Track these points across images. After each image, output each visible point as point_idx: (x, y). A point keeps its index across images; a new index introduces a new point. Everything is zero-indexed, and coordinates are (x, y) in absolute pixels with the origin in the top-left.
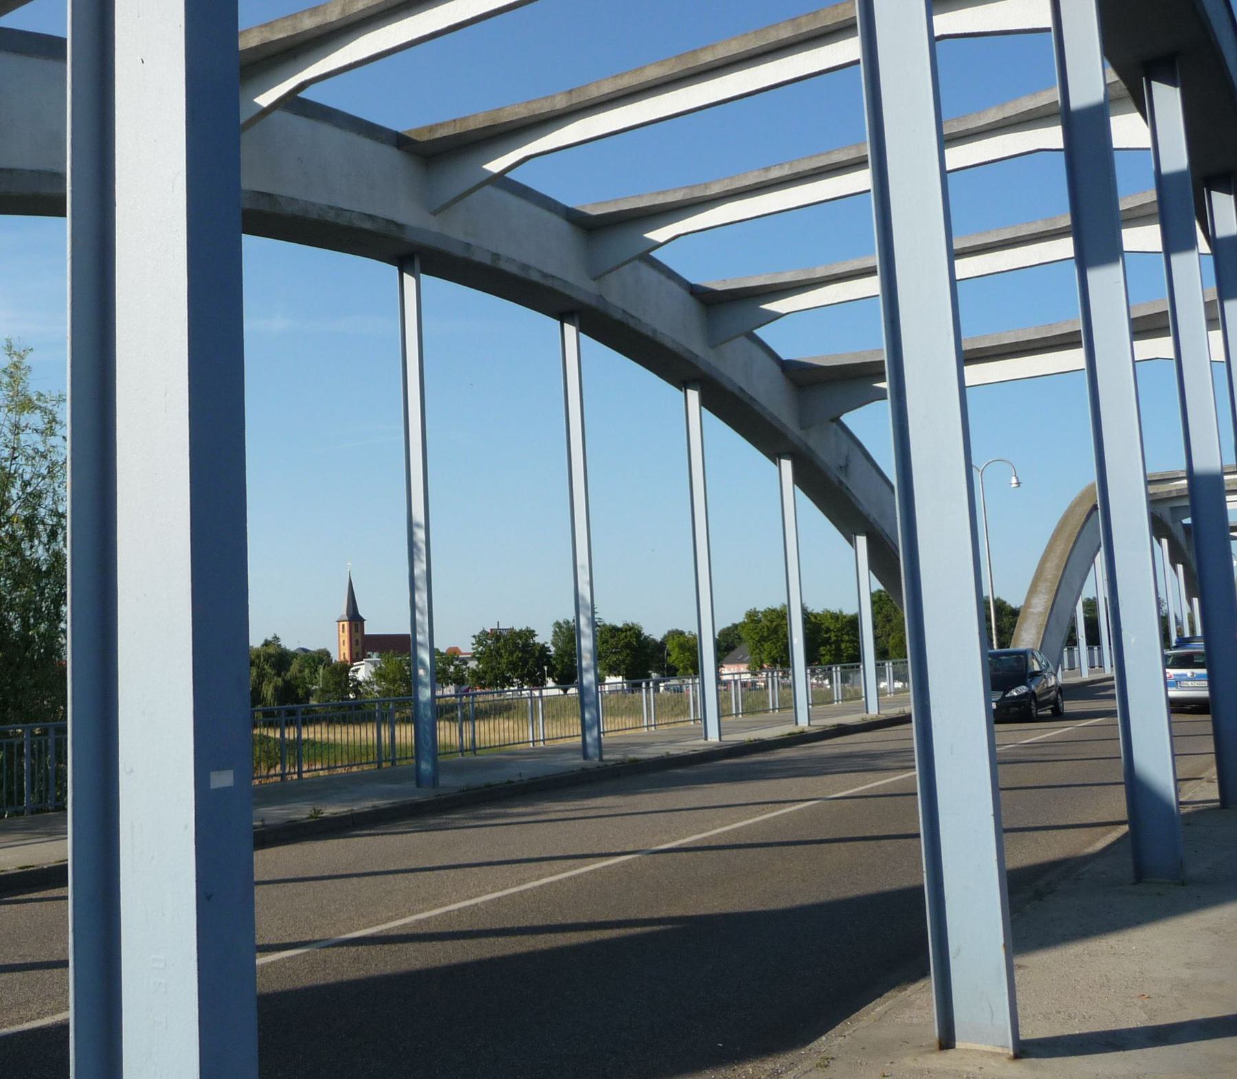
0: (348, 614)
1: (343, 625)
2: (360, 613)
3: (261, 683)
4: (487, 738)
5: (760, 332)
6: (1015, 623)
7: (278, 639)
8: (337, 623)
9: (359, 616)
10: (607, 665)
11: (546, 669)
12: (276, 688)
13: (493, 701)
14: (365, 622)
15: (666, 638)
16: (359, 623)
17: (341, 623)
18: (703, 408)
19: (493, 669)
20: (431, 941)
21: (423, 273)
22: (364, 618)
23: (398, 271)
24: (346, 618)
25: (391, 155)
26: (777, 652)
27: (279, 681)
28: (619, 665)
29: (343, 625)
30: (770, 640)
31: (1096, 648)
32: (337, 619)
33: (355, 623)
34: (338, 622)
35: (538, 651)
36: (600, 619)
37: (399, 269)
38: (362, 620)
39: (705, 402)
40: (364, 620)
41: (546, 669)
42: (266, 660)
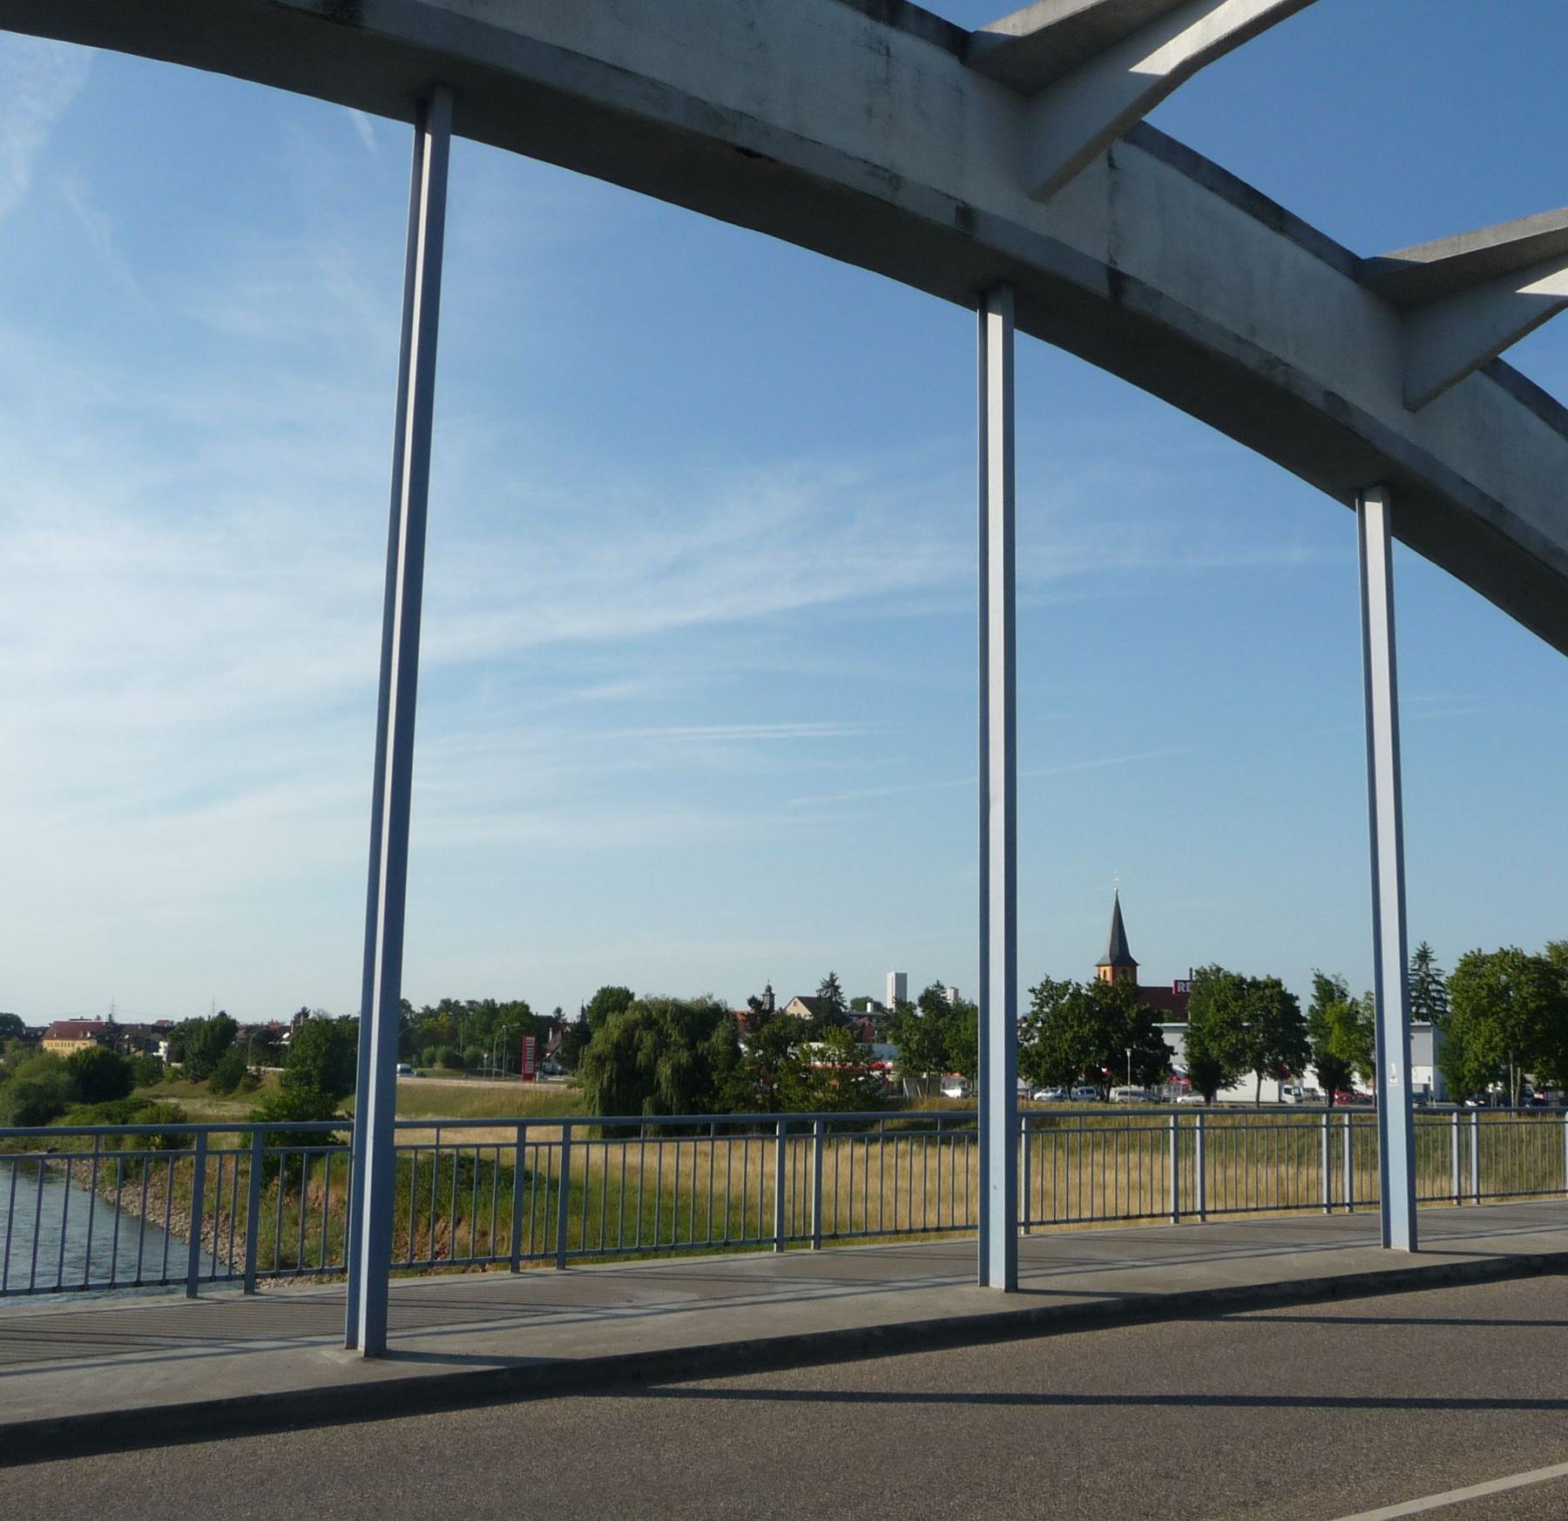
0: (1111, 955)
1: (1105, 972)
2: (1132, 955)
3: (656, 1060)
4: (844, 1180)
5: (1520, 357)
6: (180, 1034)
7: (942, 988)
8: (1097, 968)
9: (1131, 958)
10: (1222, 1051)
11: (1128, 1054)
12: (677, 1070)
13: (437, 1147)
14: (1138, 968)
15: (583, 1016)
16: (1128, 969)
17: (1102, 969)
18: (1396, 544)
19: (1053, 1049)
20: (1177, 1396)
21: (1018, 329)
22: (1138, 962)
23: (414, 131)
24: (1108, 961)
25: (941, 62)
26: (1502, 1040)
27: (684, 1057)
28: (1242, 1052)
29: (1105, 972)
30: (1493, 1014)
31: (242, 1291)
32: (1096, 962)
33: (1121, 969)
34: (1099, 966)
35: (1134, 1020)
36: (1440, 970)
37: (416, 128)
38: (1133, 965)
39: (1395, 527)
40: (1137, 965)
41: (1128, 1054)
42: (675, 1020)
